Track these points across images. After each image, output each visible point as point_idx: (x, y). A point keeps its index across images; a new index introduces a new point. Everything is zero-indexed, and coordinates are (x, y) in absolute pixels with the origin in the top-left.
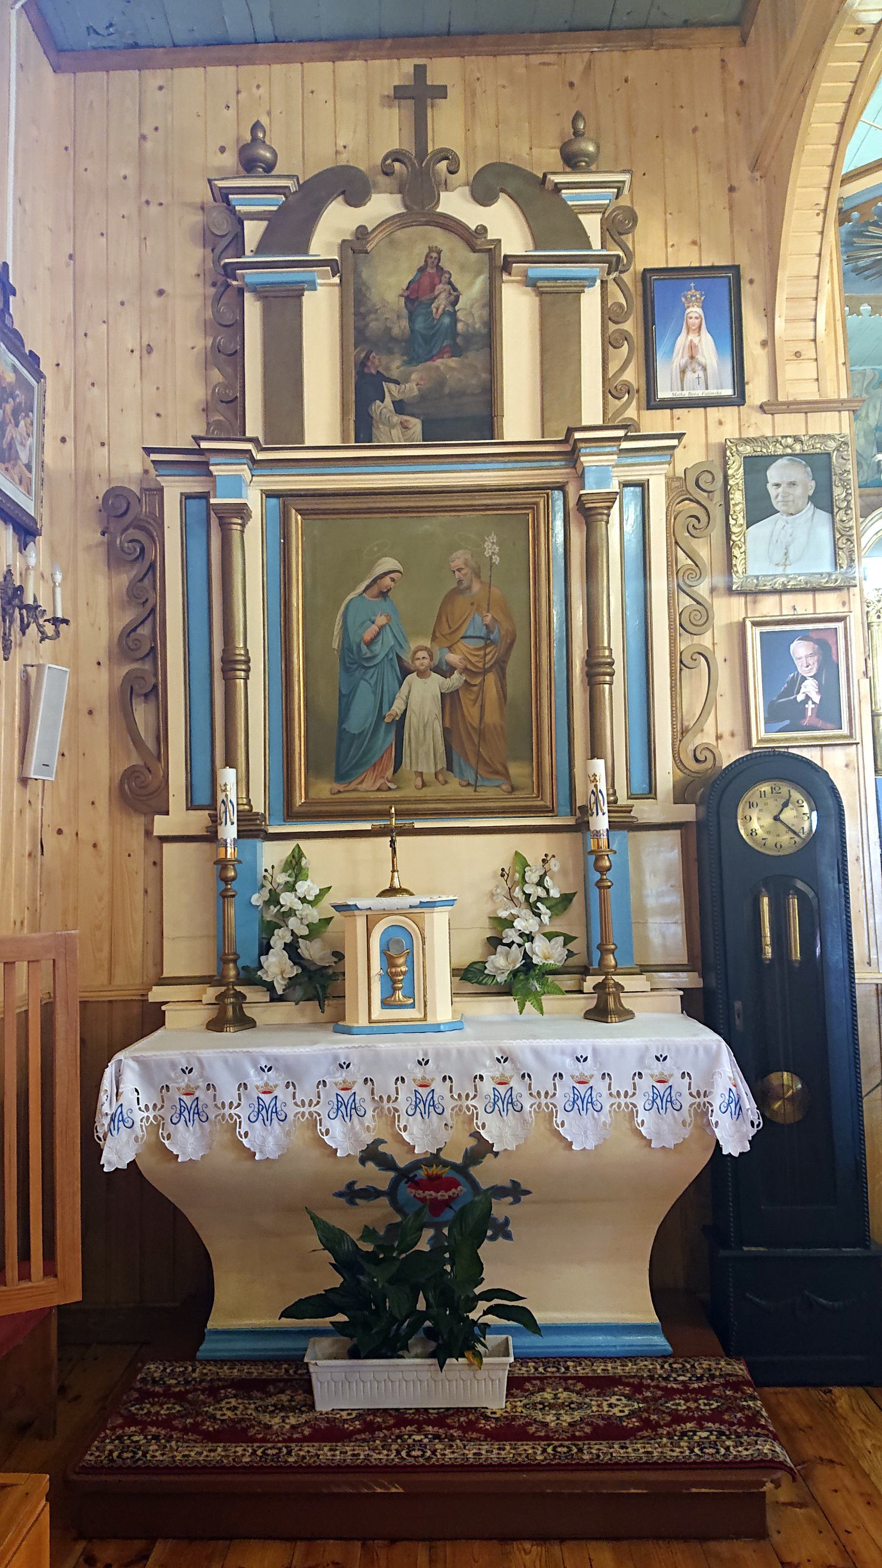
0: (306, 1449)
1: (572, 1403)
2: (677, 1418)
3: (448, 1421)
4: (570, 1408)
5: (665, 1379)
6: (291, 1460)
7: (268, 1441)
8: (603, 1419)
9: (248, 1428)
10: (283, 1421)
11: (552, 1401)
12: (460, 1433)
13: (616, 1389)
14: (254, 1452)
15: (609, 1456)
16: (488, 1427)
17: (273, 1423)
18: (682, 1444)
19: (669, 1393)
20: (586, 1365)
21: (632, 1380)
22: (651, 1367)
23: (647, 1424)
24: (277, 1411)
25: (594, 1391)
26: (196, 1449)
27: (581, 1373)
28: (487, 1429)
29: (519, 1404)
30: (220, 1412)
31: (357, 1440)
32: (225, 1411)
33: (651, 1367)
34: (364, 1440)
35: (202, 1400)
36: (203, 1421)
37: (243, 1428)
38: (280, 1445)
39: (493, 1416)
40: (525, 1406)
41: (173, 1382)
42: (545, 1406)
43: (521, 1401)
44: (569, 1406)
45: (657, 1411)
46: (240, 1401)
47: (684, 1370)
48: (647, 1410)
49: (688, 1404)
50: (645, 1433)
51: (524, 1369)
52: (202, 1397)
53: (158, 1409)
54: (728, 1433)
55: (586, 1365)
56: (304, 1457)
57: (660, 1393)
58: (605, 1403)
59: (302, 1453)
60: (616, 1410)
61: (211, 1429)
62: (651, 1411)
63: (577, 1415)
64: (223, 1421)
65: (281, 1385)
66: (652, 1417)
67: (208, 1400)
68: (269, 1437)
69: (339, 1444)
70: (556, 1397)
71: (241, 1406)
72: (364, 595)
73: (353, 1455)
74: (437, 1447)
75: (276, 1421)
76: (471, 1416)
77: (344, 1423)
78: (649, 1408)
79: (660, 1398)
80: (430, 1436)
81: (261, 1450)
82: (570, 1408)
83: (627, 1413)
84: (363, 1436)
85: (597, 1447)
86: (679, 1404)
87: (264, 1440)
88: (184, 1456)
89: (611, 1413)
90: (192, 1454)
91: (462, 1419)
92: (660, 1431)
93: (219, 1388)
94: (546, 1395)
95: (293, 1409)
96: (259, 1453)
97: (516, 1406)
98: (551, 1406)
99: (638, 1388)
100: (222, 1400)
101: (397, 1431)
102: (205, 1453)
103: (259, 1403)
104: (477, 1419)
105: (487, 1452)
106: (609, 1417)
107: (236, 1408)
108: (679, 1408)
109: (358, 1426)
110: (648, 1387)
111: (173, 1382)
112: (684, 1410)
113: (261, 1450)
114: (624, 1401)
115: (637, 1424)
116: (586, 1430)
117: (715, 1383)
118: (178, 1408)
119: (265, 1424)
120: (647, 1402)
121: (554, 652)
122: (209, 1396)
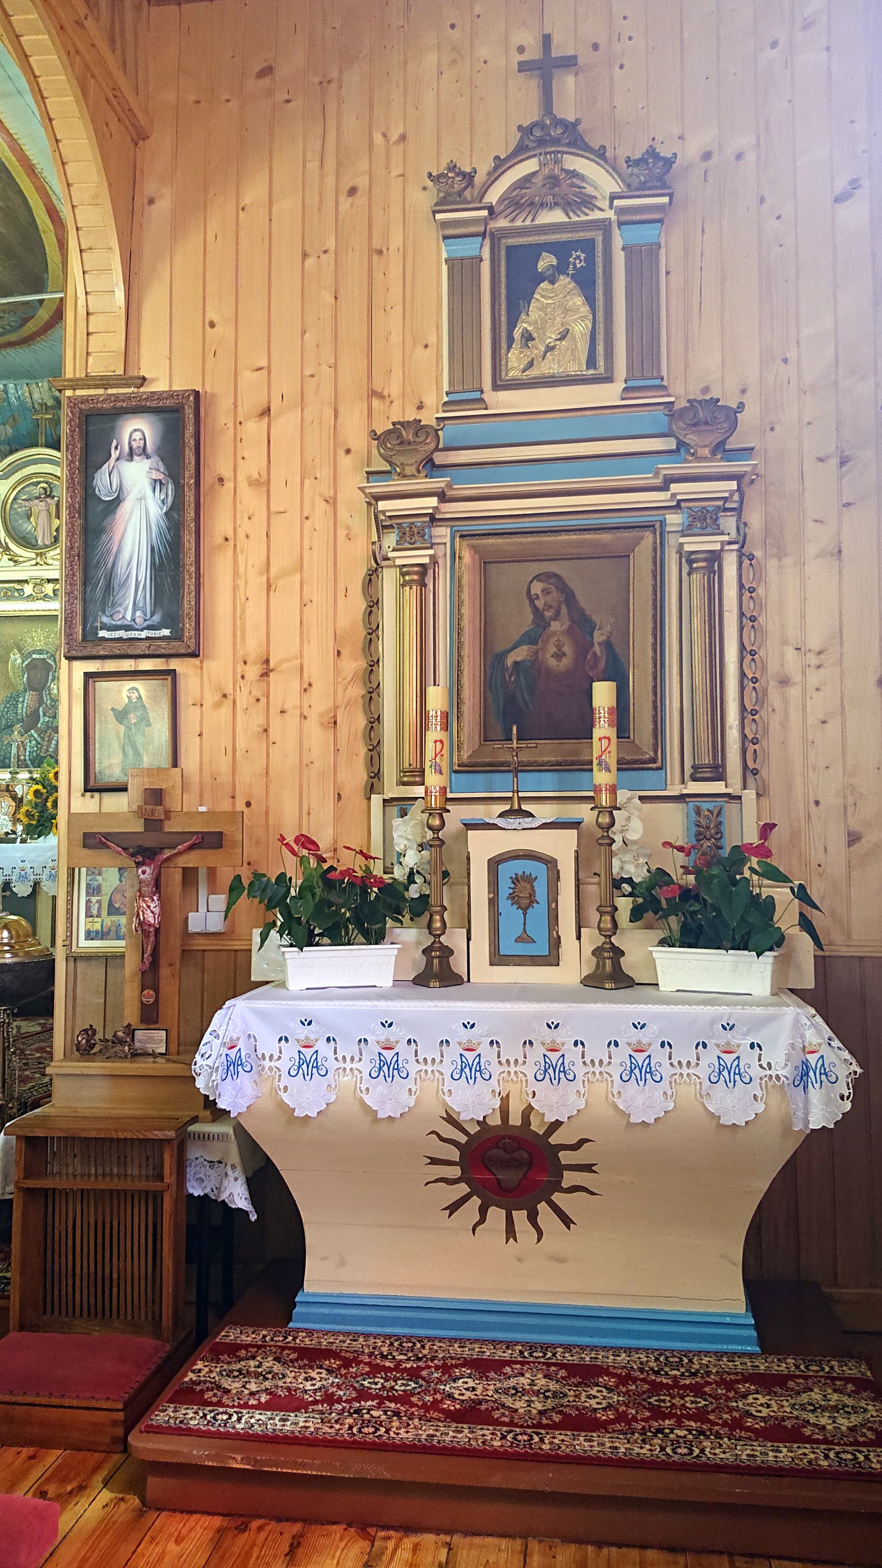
0: (249, 1339)
1: (813, 1411)
2: (697, 1390)
3: (647, 1386)
4: (814, 1406)
5: (702, 1433)
6: (264, 1332)
7: (280, 1347)
8: (775, 1393)
9: (297, 1360)
10: (261, 1363)
11: (534, 1399)
12: (361, 1358)
13: (762, 1424)
14: (294, 1339)
15: (768, 1360)
16: (606, 1378)
17: (544, 1380)
18: (698, 1367)
19: (701, 1416)
20: (801, 1460)
21: (743, 1434)
22: (718, 1451)
23: (729, 1385)
24: (542, 1391)
25: (788, 1424)
26: (346, 1345)
27: (807, 1449)
28: (606, 1376)
29: (571, 1399)
30: (322, 1376)
31: (459, 1359)
32: (317, 1377)
33: (718, 1451)
34: (452, 1358)
35: (341, 1390)
36: (339, 1369)
37: (302, 1360)
38: (532, 1359)
39: (600, 1388)
40: (565, 1395)
41: (375, 1413)
42: (517, 1392)
43: (569, 1401)
44: (517, 1392)
45: (716, 1397)
46: (301, 1386)
47: (676, 1444)
48: (728, 1399)
49: (682, 1402)
50: (732, 1377)
51: (556, 1441)
52: (341, 1393)
53: (385, 1384)
54: (650, 1372)
55: (801, 1460)
56: (253, 1333)
57: (712, 1417)
58: (775, 1409)
59: (510, 1352)
60: (762, 1400)
61: (332, 1361)
62: (724, 1398)
63: (804, 1398)
64: (321, 1367)
65: (252, 1402)
66: (724, 1392)
67: (335, 1389)
68: (544, 1367)
69: (475, 1357)
70: (529, 1402)
71: (300, 1381)
72: (299, 661)
73: (463, 1347)
74: (655, 1364)
75: (541, 1382)
76: (624, 1390)
77: (470, 1374)
78: (726, 1401)
79: (713, 1411)
80: (663, 1373)
81: (548, 1356)
82: (814, 1406)
83: (750, 1397)
84: (453, 1362)
85: (781, 1368)
86: (692, 1402)
87: (283, 1348)
88: (356, 1340)
89: (768, 1398)
90: (348, 1342)
91: (633, 1387)
92: (718, 1379)
93: (322, 1402)
94: (539, 1406)
95: (257, 1375)
96: (290, 1338)
97: (575, 1396)
98: (524, 1392)
99: (736, 1424)
100: (320, 1389)
101: (420, 1364)
102: (337, 1341)
103: (280, 1383)
104: (617, 1386)
105: (608, 1358)
106: (769, 1394)
107: (306, 1379)
108: (692, 1399)
109: (457, 1370)
110: (725, 1424)
111: (375, 1413)
112: (688, 1395)
113: (548, 1356)
114: (753, 1410)
115: (740, 1386)
116: (793, 1383)
117: (644, 1424)
118: (366, 1383)
119: (279, 1362)
120: (728, 1407)
121: (696, 671)
122: (333, 1394)
